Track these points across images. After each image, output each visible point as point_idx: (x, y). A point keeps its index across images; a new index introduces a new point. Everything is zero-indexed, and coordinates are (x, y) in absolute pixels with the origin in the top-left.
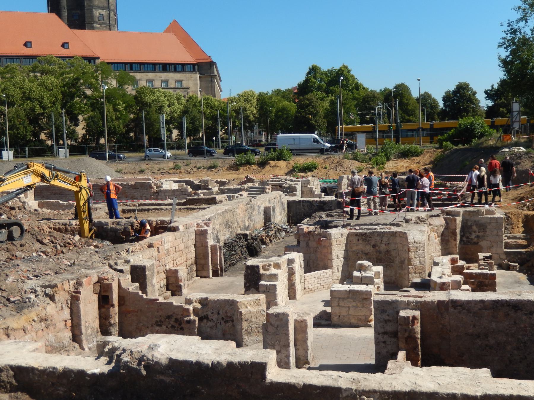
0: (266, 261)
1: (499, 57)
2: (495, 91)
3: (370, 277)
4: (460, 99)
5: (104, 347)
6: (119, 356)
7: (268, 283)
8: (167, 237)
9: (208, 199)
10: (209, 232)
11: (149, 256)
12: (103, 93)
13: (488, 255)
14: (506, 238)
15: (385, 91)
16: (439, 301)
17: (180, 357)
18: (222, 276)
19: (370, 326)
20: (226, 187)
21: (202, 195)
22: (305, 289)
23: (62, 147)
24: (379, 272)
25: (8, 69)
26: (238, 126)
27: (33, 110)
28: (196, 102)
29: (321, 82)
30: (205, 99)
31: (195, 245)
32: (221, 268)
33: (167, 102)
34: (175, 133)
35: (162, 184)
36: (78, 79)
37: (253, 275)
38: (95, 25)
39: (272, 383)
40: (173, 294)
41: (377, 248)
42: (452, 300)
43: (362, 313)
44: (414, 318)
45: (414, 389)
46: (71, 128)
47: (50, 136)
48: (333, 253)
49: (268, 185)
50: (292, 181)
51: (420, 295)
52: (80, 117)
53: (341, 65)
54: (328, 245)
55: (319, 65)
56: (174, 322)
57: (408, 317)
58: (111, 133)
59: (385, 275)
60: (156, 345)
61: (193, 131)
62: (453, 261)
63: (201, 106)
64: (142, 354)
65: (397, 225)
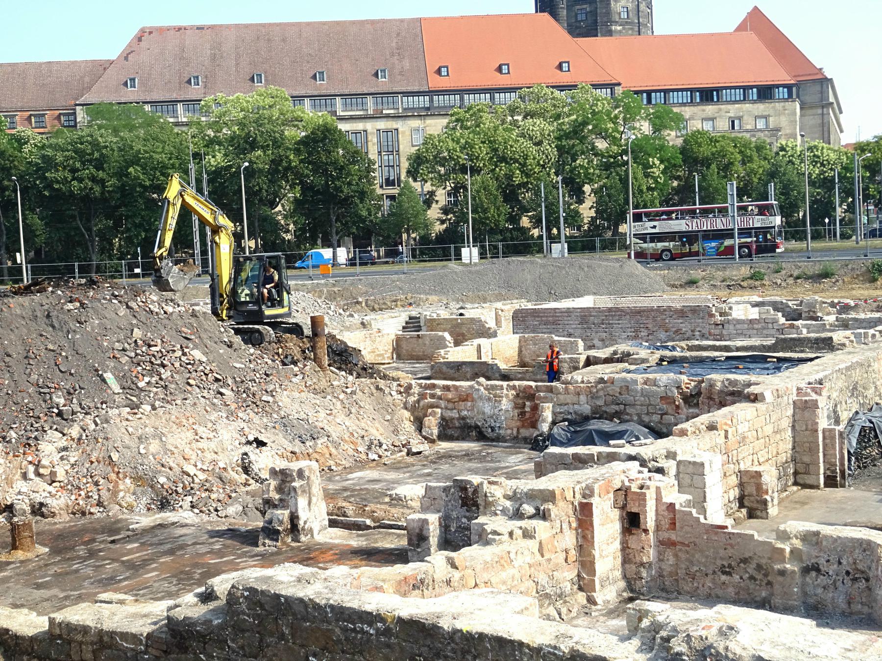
6: (667, 640)
8: (742, 410)
9: (817, 339)
10: (820, 405)
11: (708, 446)
12: (627, 145)
21: (805, 331)
23: (554, 239)
25: (471, 112)
27: (509, 177)
28: (792, 156)
30: (810, 149)
31: (793, 427)
32: (843, 472)
33: (738, 156)
35: (730, 308)
36: (585, 123)
38: (613, 28)
40: (751, 515)
46: (572, 207)
47: (537, 222)
52: (587, 188)
63: (802, 161)
64: (708, 643)
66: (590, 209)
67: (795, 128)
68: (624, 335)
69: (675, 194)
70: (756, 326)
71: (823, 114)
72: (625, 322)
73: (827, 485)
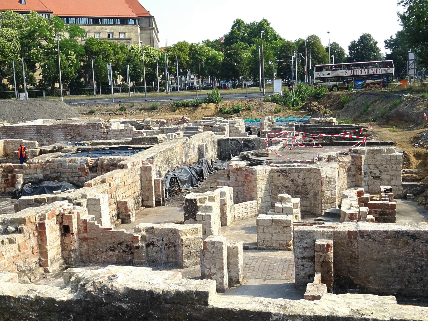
0: (202, 195)
1: (398, 14)
2: (393, 41)
3: (290, 207)
4: (363, 48)
5: (70, 277)
6: (84, 285)
7: (204, 214)
8: (117, 173)
10: (153, 169)
11: (102, 190)
12: (57, 43)
13: (388, 187)
14: (404, 173)
15: (299, 41)
16: (349, 231)
17: (135, 286)
18: (164, 205)
19: (290, 250)
20: (165, 127)
21: (145, 134)
22: (234, 217)
23: (22, 90)
24: (297, 203)
26: (174, 72)
28: (137, 52)
29: (244, 34)
32: (163, 199)
33: (112, 51)
34: (120, 78)
35: (111, 124)
36: (35, 31)
37: (192, 207)
39: (213, 309)
40: (123, 222)
41: (295, 182)
42: (360, 231)
43: (282, 238)
44: (328, 246)
45: (332, 314)
46: (30, 74)
47: (11, 81)
48: (258, 187)
49: (201, 125)
50: (221, 121)
51: (333, 226)
52: (37, 65)
53: (262, 19)
54: (254, 179)
55: (242, 19)
56: (127, 253)
57: (323, 245)
58: (65, 78)
59: (301, 205)
60: (114, 276)
61: (135, 78)
62: (360, 194)
64: (103, 284)
65: (312, 162)
66: (39, 75)
67: (138, 39)
68: (59, 139)
69: (82, 69)
70: (123, 133)
71: (150, 33)
72: (59, 132)
73: (156, 205)
